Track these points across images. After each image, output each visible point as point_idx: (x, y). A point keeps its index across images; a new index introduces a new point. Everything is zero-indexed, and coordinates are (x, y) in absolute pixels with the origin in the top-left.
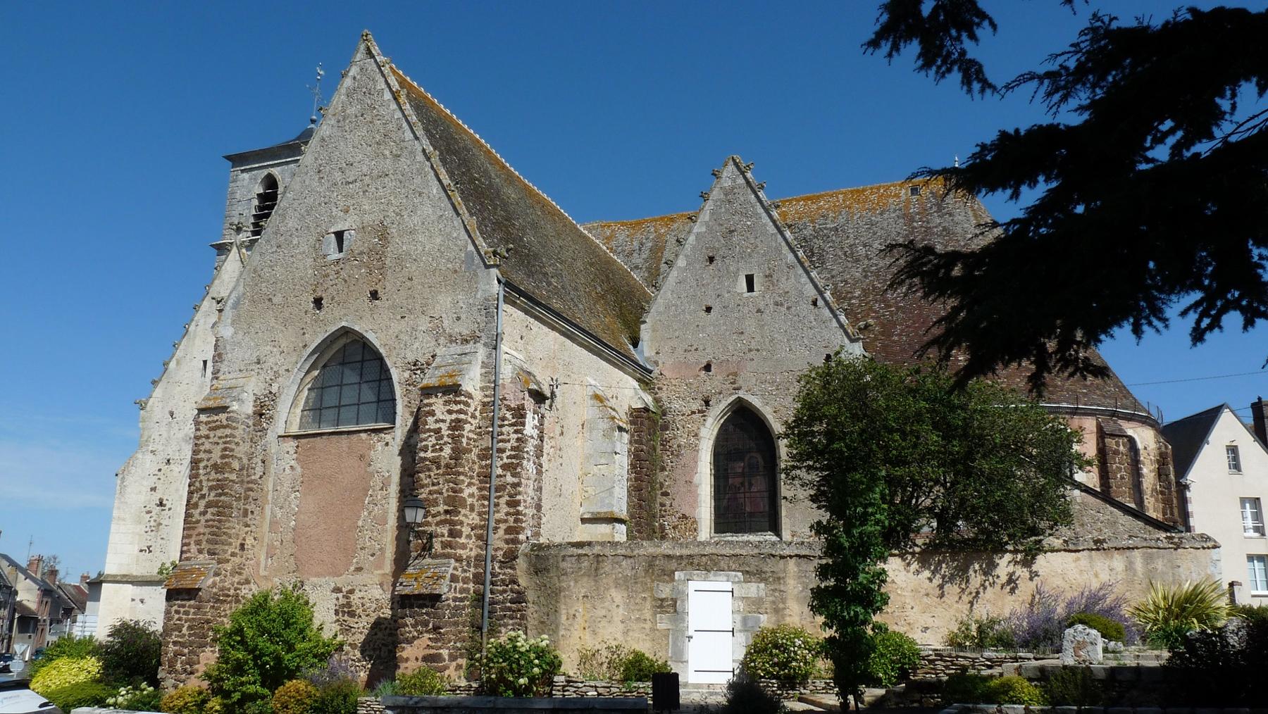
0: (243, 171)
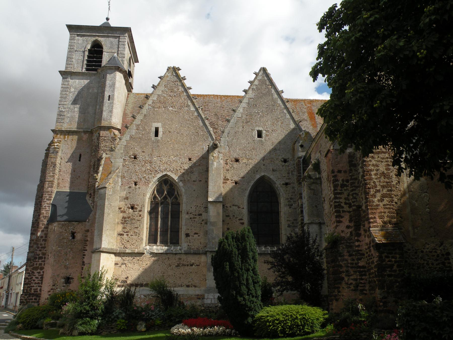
0: (78, 35)
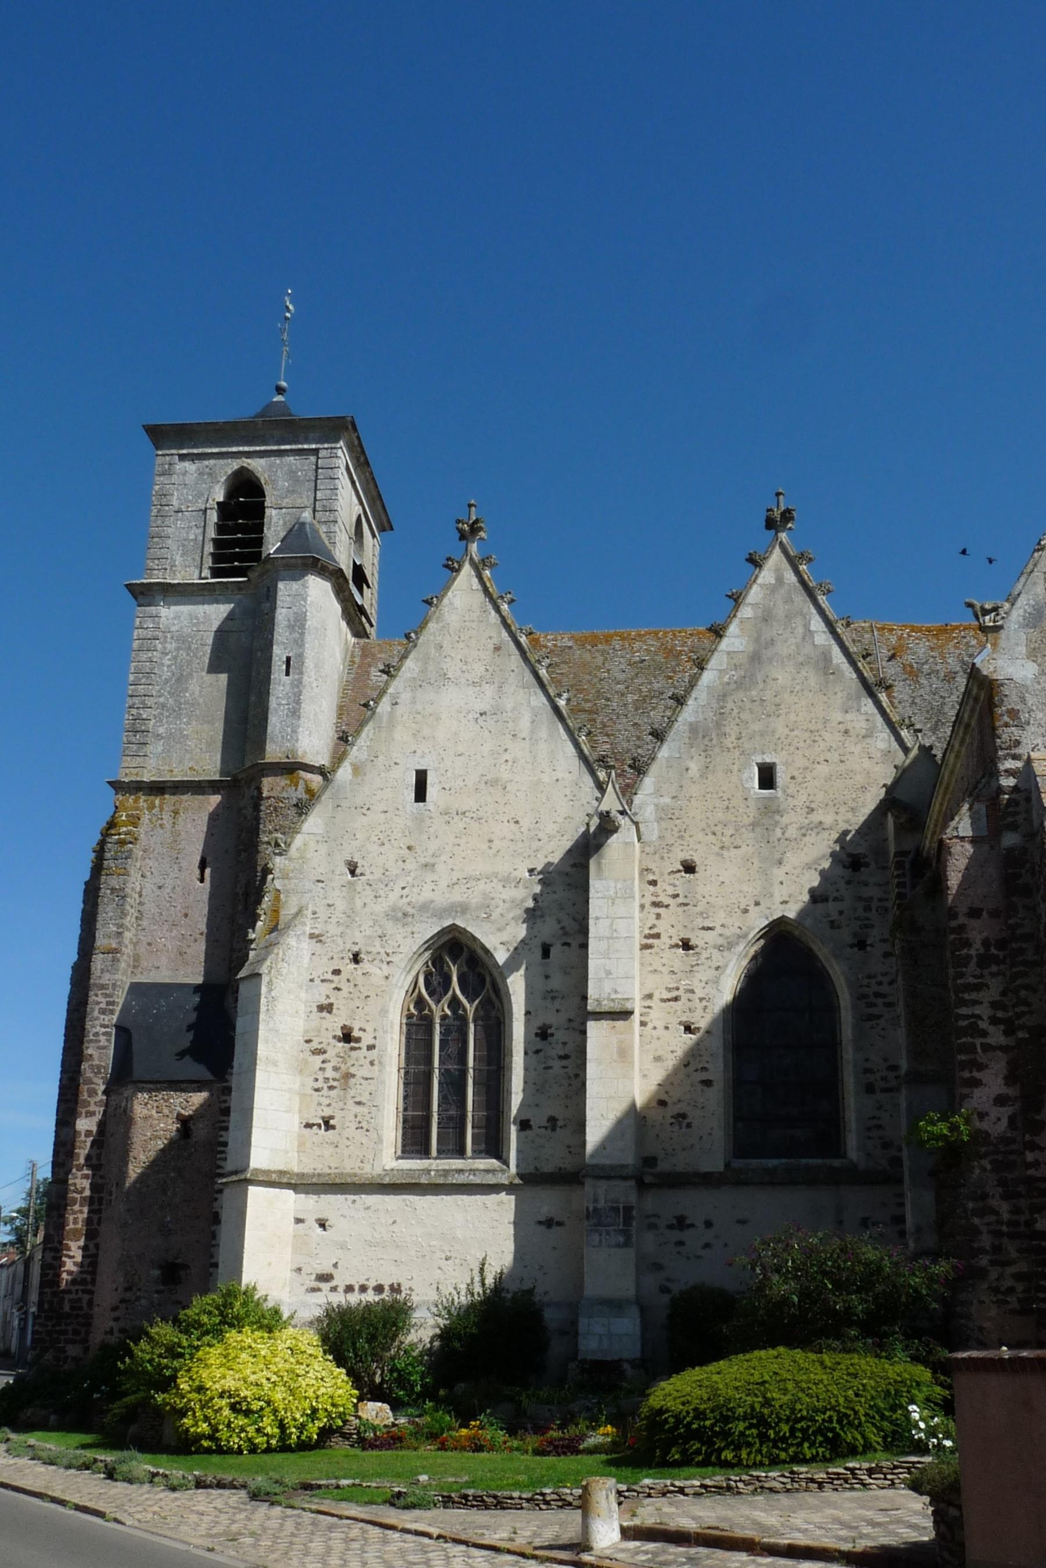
0: (182, 457)
